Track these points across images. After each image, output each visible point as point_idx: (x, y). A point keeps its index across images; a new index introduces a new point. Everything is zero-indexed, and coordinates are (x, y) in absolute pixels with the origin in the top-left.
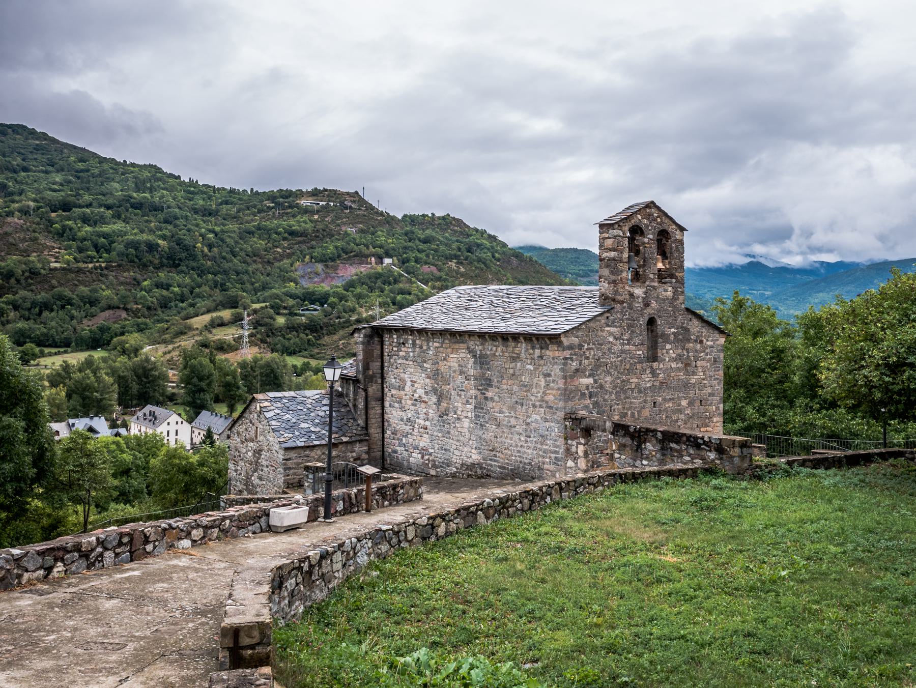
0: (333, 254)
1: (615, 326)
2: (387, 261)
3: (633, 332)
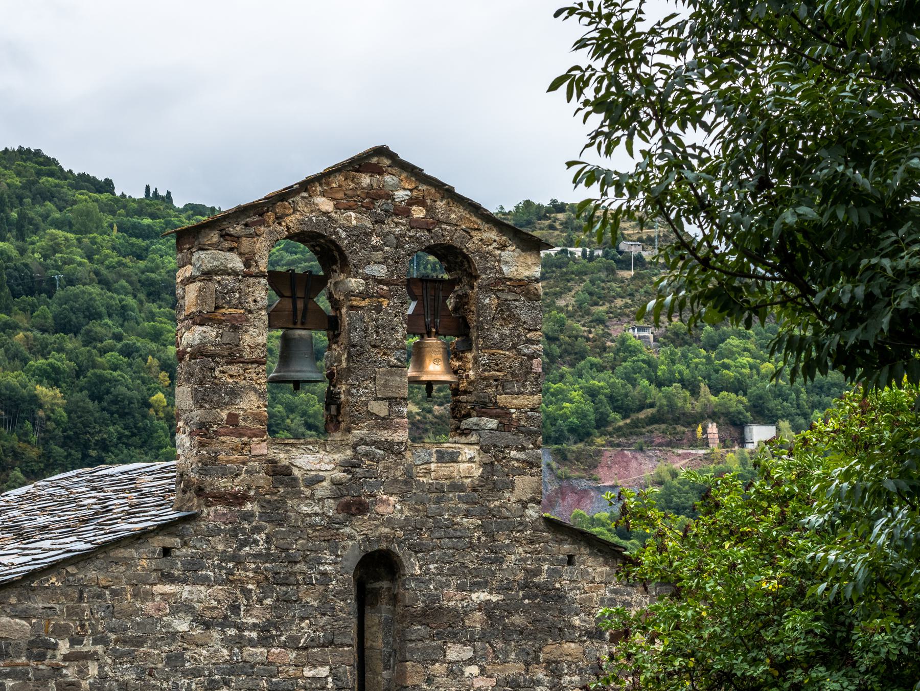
0: (583, 415)
1: (205, 581)
2: (759, 433)
3: (286, 600)
